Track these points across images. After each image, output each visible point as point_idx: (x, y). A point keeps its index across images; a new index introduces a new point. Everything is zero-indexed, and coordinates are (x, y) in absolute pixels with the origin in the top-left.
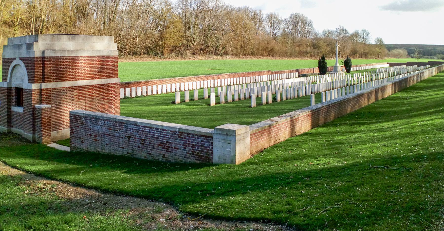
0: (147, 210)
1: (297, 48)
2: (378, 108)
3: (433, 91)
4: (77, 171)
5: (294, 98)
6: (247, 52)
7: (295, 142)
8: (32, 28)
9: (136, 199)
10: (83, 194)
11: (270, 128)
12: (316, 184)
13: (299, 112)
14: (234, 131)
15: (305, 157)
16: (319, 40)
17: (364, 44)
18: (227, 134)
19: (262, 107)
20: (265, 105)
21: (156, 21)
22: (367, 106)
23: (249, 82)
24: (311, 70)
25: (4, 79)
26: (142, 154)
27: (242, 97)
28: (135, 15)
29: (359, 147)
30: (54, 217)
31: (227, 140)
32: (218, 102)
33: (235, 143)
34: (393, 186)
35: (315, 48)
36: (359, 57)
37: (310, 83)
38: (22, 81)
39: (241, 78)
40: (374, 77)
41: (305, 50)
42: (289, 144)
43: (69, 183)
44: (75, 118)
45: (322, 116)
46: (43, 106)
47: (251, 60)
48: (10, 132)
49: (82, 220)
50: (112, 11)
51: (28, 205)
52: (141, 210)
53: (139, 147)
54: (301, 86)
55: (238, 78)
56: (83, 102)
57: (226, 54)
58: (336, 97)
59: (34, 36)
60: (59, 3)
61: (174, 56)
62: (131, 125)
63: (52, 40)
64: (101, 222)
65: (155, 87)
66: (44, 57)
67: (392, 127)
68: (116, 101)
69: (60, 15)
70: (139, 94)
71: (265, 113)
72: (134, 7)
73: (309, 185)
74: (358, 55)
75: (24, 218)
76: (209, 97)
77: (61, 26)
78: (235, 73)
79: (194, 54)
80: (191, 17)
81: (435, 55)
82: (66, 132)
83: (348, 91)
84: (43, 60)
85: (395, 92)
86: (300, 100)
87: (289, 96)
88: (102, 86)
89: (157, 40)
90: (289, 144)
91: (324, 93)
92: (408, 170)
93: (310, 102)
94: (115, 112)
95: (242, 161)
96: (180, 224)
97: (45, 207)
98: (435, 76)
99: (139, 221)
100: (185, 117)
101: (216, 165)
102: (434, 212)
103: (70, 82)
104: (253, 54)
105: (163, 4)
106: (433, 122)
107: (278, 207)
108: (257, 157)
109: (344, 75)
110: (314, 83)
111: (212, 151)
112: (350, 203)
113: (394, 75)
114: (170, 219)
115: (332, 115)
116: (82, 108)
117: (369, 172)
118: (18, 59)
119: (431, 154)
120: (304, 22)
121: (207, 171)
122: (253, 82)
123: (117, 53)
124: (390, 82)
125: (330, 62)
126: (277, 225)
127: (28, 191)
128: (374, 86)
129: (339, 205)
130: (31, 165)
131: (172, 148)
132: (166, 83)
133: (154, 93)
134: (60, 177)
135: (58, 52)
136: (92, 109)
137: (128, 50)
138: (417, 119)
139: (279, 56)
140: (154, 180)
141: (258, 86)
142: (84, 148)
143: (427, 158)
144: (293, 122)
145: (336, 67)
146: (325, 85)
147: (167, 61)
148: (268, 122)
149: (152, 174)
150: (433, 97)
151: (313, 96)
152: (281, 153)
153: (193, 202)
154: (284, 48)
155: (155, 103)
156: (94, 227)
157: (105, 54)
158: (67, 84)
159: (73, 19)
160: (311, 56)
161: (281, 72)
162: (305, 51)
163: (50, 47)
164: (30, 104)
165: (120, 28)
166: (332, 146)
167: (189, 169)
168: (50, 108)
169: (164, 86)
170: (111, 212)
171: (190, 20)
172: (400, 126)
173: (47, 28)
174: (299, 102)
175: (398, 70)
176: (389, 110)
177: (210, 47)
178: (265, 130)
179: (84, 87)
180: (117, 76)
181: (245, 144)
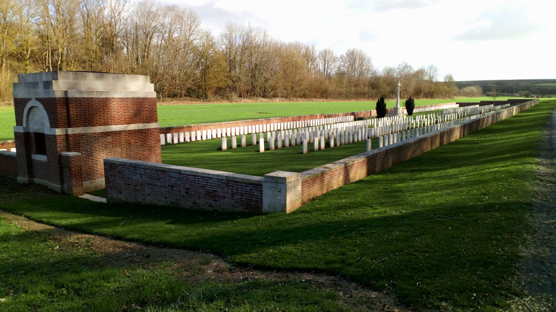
0: (193, 262)
1: (353, 89)
2: (443, 153)
3: (512, 134)
4: (115, 223)
5: (349, 143)
6: (298, 94)
7: (349, 190)
8: (49, 63)
9: (182, 251)
10: (123, 247)
11: (323, 175)
12: (371, 233)
13: (353, 158)
14: (284, 179)
15: (359, 206)
17: (430, 82)
18: (277, 182)
19: (314, 153)
20: (317, 151)
21: (197, 58)
22: (430, 152)
23: (301, 127)
25: (19, 122)
26: (187, 204)
27: (293, 142)
28: (172, 51)
29: (419, 195)
30: (89, 273)
31: (277, 188)
32: (267, 148)
33: (286, 191)
34: (457, 237)
35: (373, 88)
36: (423, 97)
37: (367, 126)
38: (43, 125)
39: (292, 123)
40: (440, 119)
42: (343, 192)
43: (106, 237)
44: (109, 166)
45: (378, 163)
48: (31, 184)
49: (122, 275)
50: (146, 46)
51: (59, 262)
52: (187, 262)
53: (184, 197)
54: (357, 130)
55: (289, 123)
57: (275, 96)
58: (395, 142)
59: (51, 72)
60: (79, 34)
61: (219, 98)
62: (174, 173)
63: (76, 78)
64: (143, 276)
65: (199, 133)
66: (68, 98)
67: (458, 174)
69: (82, 48)
70: (188, 140)
71: (317, 160)
72: (171, 41)
73: (364, 234)
74: (422, 94)
75: (54, 277)
76: (258, 143)
77: (84, 62)
78: (285, 117)
79: (240, 96)
80: (236, 54)
81: (517, 91)
82: (101, 181)
83: (409, 135)
84: (66, 101)
85: (464, 136)
86: (355, 145)
87: (343, 141)
89: (199, 81)
90: (343, 192)
91: (381, 138)
92: (476, 221)
93: (366, 147)
94: (155, 160)
95: (293, 210)
96: (229, 275)
97: (79, 264)
98: (515, 116)
99: (185, 273)
100: (233, 164)
101: (266, 214)
102: (506, 267)
103: (102, 127)
104: (304, 96)
105: (204, 38)
106: (509, 168)
107: (330, 257)
108: (308, 205)
109: (405, 118)
110: (371, 127)
111: (261, 199)
112: (408, 254)
113: (464, 117)
114: (218, 271)
115: (391, 160)
116: (118, 155)
117: (430, 222)
119: (505, 204)
120: (362, 59)
121: (256, 220)
122: (305, 127)
123: (154, 95)
124: (458, 124)
125: (389, 104)
126: (329, 275)
127: (58, 247)
128: (439, 129)
129: (397, 255)
130: (60, 218)
131: (219, 196)
132: (210, 129)
133: (198, 139)
134: (96, 230)
135: (84, 92)
136: (129, 156)
137: (167, 91)
138: (488, 166)
140: (201, 230)
141: (310, 131)
142: (123, 199)
143: (499, 208)
144: (347, 169)
145: (396, 109)
146: (383, 129)
148: (321, 169)
149: (198, 224)
150: (510, 140)
151: (370, 141)
152: (334, 201)
153: (243, 252)
154: (339, 89)
155: (200, 149)
156: (135, 282)
157: (141, 96)
158: (99, 129)
159: (99, 54)
160: (368, 98)
161: (335, 116)
162: (362, 91)
163: (74, 86)
165: (156, 66)
166: (390, 194)
167: (238, 218)
168: (80, 156)
169: (209, 131)
170: (155, 265)
171: (235, 57)
172: (468, 173)
173: (68, 64)
174: (354, 147)
175: (469, 111)
176: (455, 155)
177: (258, 89)
178: (317, 177)
179: (119, 133)
180: (156, 121)
181: (296, 193)
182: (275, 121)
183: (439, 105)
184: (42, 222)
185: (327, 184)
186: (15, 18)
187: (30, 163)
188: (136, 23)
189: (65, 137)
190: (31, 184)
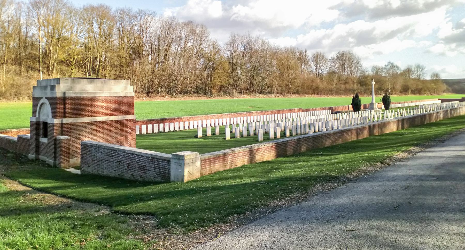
1: (343, 86)
14: (183, 156)
16: (366, 78)
17: (418, 80)
24: (346, 107)
25: (34, 114)
26: (127, 176)
36: (412, 93)
38: (48, 116)
39: (270, 116)
41: (351, 88)
46: (62, 137)
47: (295, 98)
48: (37, 159)
56: (101, 135)
57: (271, 92)
68: (132, 134)
70: (177, 129)
74: (410, 91)
78: (265, 111)
79: (241, 93)
84: (64, 99)
85: (403, 128)
88: (119, 121)
89: (206, 80)
103: (90, 118)
104: (297, 93)
118: (44, 98)
123: (133, 94)
125: (364, 100)
135: (78, 93)
136: (109, 141)
139: (324, 94)
145: (371, 105)
147: (216, 99)
157: (122, 95)
158: (86, 120)
163: (71, 88)
164: (53, 135)
179: (102, 123)
180: (133, 114)
181: (193, 168)
182: (256, 114)
183: (419, 101)
184: (25, 185)
185: (230, 163)
187: (38, 144)
188: (159, 36)
189: (60, 125)
190: (37, 159)
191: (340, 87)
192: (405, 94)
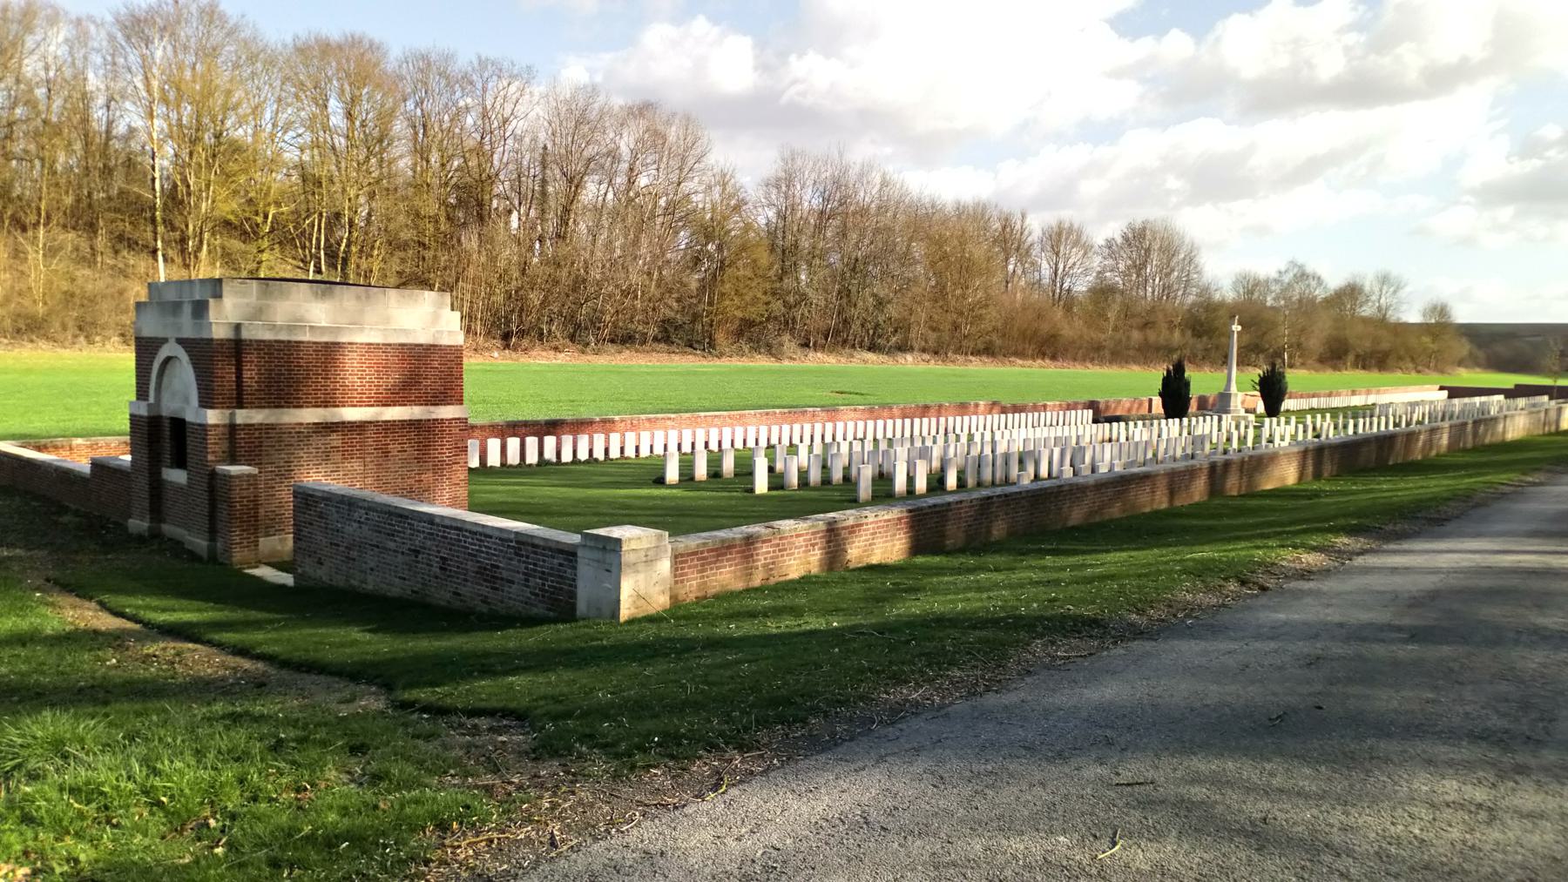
1: (1136, 335)
4: (257, 625)
8: (318, 248)
14: (618, 541)
17: (1381, 322)
24: (1141, 404)
25: (142, 393)
36: (1355, 366)
38: (187, 400)
39: (899, 422)
41: (1162, 341)
46: (234, 469)
48: (155, 535)
56: (356, 465)
57: (903, 348)
68: (455, 467)
70: (599, 454)
74: (1351, 358)
78: (883, 406)
79: (806, 345)
84: (237, 348)
85: (1317, 475)
89: (694, 301)
103: (321, 411)
104: (988, 351)
123: (458, 339)
125: (1201, 381)
133: (627, 454)
136: (382, 486)
137: (508, 327)
139: (1075, 360)
147: (724, 363)
154: (1095, 335)
158: (310, 415)
161: (1035, 408)
163: (258, 313)
179: (361, 426)
180: (460, 402)
181: (648, 577)
182: (852, 415)
183: (1378, 392)
185: (765, 566)
186: (241, 131)
187: (157, 488)
188: (545, 148)
189: (226, 431)
190: (155, 535)
191: (1128, 338)
192: (1336, 368)
